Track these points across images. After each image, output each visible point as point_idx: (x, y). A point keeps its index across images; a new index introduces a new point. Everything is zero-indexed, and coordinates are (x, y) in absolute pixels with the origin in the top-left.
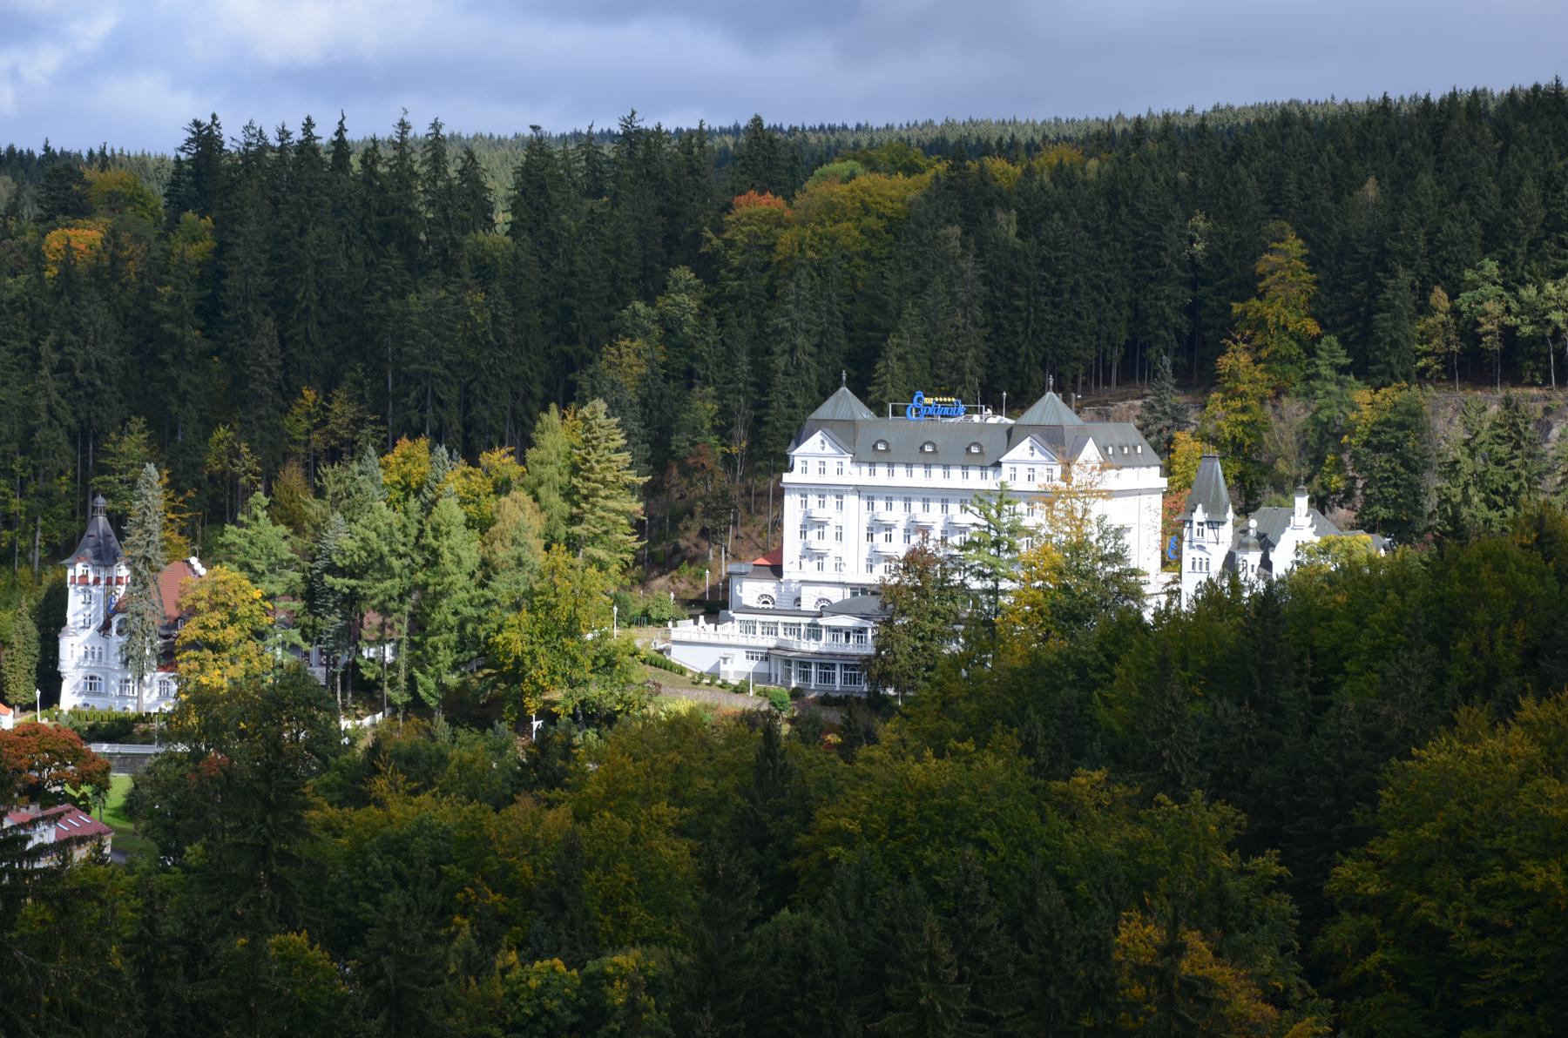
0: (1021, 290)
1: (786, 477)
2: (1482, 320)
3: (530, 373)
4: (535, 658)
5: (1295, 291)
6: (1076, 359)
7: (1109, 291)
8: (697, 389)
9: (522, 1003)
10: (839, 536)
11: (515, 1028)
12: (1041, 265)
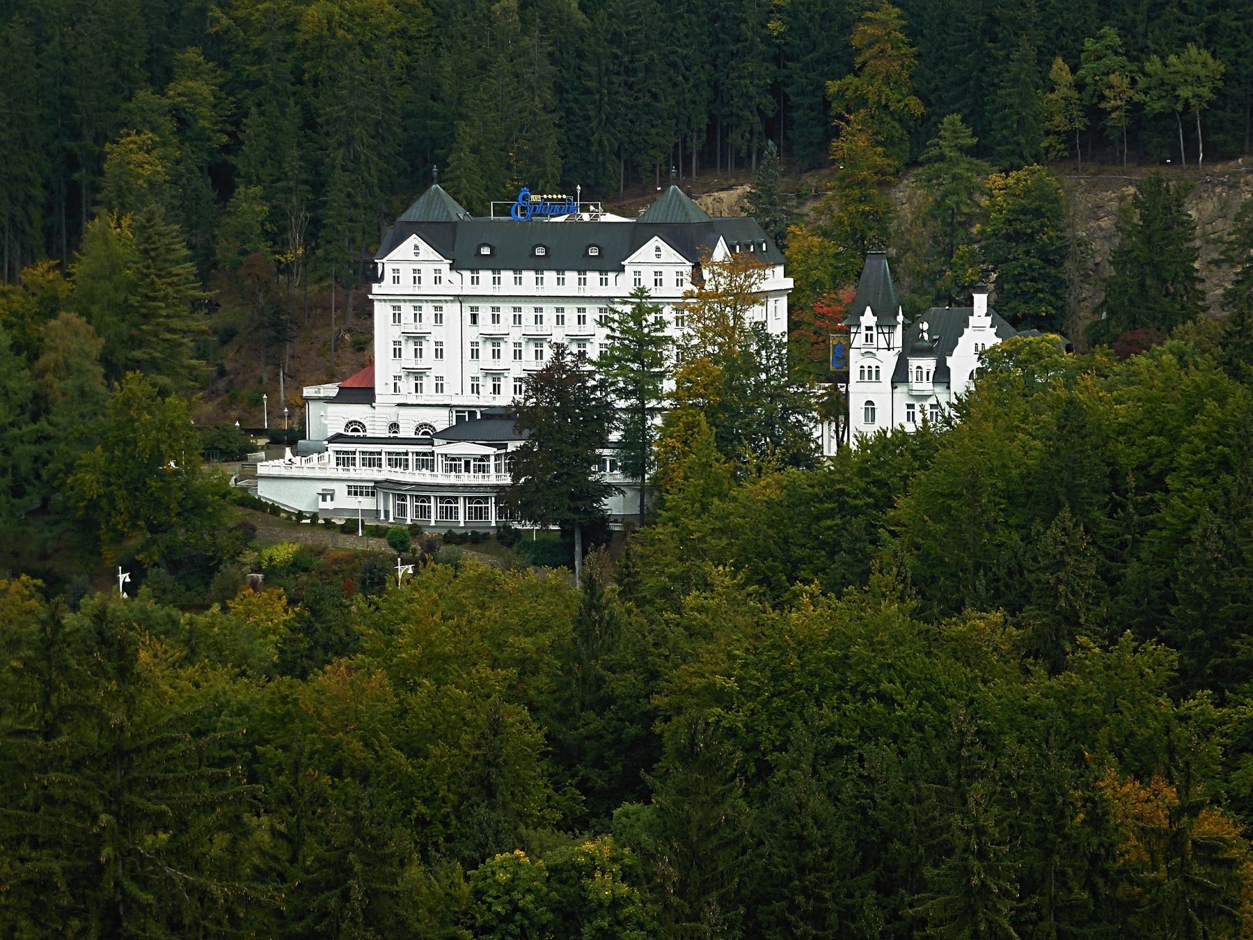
0: (592, 69)
1: (375, 288)
2: (1107, 92)
3: (30, 174)
4: (114, 500)
5: (896, 65)
6: (654, 147)
7: (687, 69)
8: (242, 189)
9: (489, 900)
10: (439, 354)
11: (487, 929)
12: (611, 42)
